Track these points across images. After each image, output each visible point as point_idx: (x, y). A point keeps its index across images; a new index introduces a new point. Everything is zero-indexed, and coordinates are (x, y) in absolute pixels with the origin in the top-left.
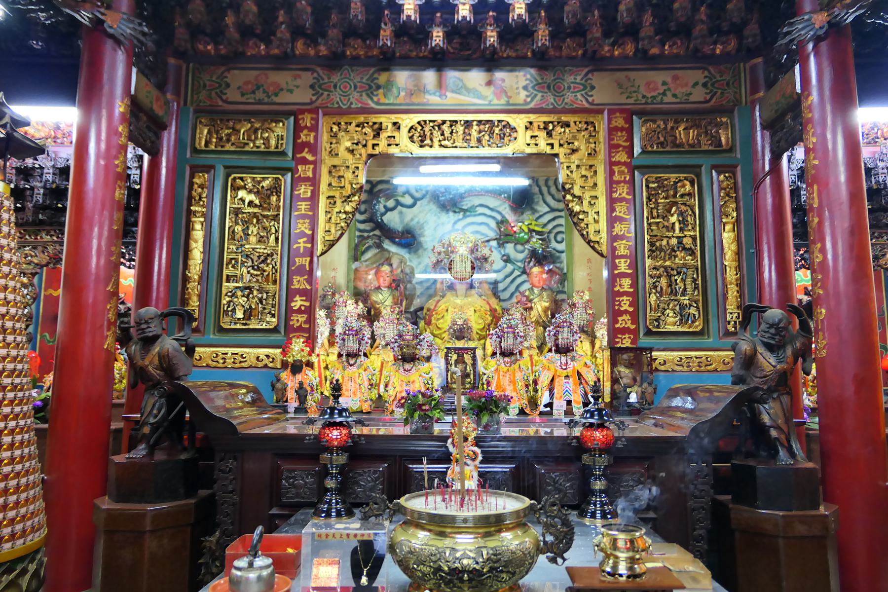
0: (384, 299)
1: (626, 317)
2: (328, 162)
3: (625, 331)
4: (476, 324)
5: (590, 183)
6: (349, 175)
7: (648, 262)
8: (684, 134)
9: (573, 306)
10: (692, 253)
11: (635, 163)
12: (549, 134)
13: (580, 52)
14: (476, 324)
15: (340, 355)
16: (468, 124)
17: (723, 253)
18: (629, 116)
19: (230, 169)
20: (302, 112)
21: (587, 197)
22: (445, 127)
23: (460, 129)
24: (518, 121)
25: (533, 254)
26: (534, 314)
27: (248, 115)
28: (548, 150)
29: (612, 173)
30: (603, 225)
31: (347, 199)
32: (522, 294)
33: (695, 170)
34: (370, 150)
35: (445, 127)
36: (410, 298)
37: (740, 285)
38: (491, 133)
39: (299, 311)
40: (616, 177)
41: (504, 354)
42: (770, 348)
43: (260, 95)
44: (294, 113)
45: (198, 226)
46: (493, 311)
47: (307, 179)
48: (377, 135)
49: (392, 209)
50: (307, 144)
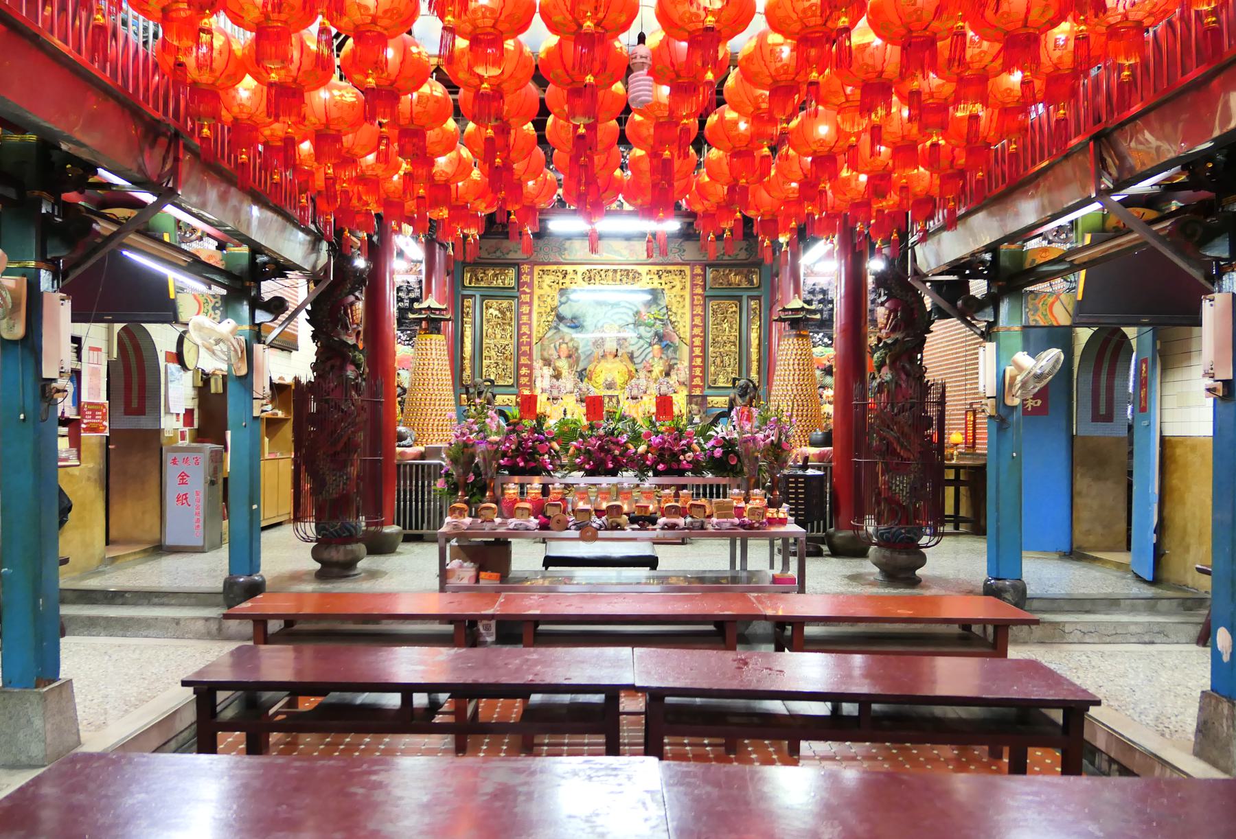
0: (563, 364)
1: (698, 379)
2: (537, 292)
3: (697, 386)
4: (619, 381)
5: (681, 305)
6: (549, 300)
7: (711, 349)
8: (735, 278)
9: (678, 369)
10: (735, 345)
11: (706, 294)
12: (660, 277)
13: (684, 203)
14: (619, 381)
15: (548, 399)
16: (615, 271)
17: (751, 345)
18: (705, 266)
19: (484, 297)
20: (523, 264)
21: (680, 312)
22: (602, 273)
23: (610, 274)
24: (643, 270)
25: (656, 334)
26: (654, 374)
27: (494, 265)
28: (659, 287)
29: (693, 300)
30: (688, 328)
31: (548, 314)
32: (647, 362)
33: (739, 298)
34: (561, 287)
35: (602, 273)
36: (577, 361)
37: (759, 361)
38: (628, 275)
39: (524, 376)
40: (696, 302)
41: (632, 398)
42: (741, 396)
43: (498, 254)
44: (516, 265)
45: (468, 329)
46: (630, 372)
47: (527, 303)
48: (564, 277)
49: (564, 303)
50: (525, 283)
